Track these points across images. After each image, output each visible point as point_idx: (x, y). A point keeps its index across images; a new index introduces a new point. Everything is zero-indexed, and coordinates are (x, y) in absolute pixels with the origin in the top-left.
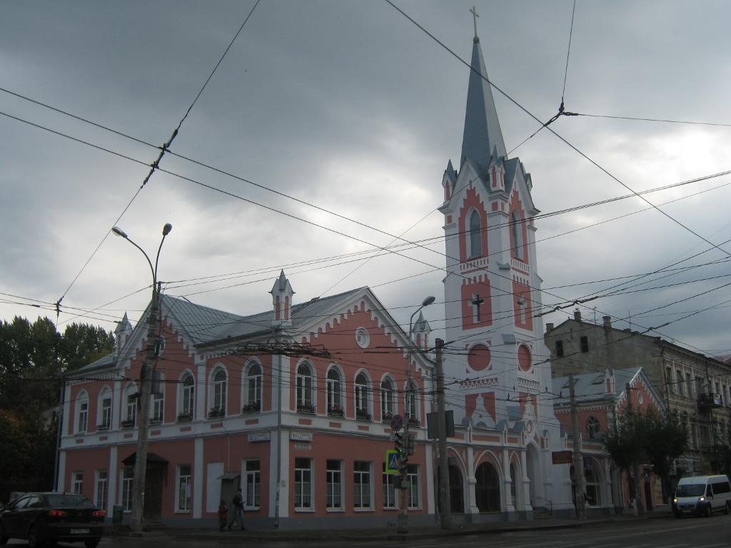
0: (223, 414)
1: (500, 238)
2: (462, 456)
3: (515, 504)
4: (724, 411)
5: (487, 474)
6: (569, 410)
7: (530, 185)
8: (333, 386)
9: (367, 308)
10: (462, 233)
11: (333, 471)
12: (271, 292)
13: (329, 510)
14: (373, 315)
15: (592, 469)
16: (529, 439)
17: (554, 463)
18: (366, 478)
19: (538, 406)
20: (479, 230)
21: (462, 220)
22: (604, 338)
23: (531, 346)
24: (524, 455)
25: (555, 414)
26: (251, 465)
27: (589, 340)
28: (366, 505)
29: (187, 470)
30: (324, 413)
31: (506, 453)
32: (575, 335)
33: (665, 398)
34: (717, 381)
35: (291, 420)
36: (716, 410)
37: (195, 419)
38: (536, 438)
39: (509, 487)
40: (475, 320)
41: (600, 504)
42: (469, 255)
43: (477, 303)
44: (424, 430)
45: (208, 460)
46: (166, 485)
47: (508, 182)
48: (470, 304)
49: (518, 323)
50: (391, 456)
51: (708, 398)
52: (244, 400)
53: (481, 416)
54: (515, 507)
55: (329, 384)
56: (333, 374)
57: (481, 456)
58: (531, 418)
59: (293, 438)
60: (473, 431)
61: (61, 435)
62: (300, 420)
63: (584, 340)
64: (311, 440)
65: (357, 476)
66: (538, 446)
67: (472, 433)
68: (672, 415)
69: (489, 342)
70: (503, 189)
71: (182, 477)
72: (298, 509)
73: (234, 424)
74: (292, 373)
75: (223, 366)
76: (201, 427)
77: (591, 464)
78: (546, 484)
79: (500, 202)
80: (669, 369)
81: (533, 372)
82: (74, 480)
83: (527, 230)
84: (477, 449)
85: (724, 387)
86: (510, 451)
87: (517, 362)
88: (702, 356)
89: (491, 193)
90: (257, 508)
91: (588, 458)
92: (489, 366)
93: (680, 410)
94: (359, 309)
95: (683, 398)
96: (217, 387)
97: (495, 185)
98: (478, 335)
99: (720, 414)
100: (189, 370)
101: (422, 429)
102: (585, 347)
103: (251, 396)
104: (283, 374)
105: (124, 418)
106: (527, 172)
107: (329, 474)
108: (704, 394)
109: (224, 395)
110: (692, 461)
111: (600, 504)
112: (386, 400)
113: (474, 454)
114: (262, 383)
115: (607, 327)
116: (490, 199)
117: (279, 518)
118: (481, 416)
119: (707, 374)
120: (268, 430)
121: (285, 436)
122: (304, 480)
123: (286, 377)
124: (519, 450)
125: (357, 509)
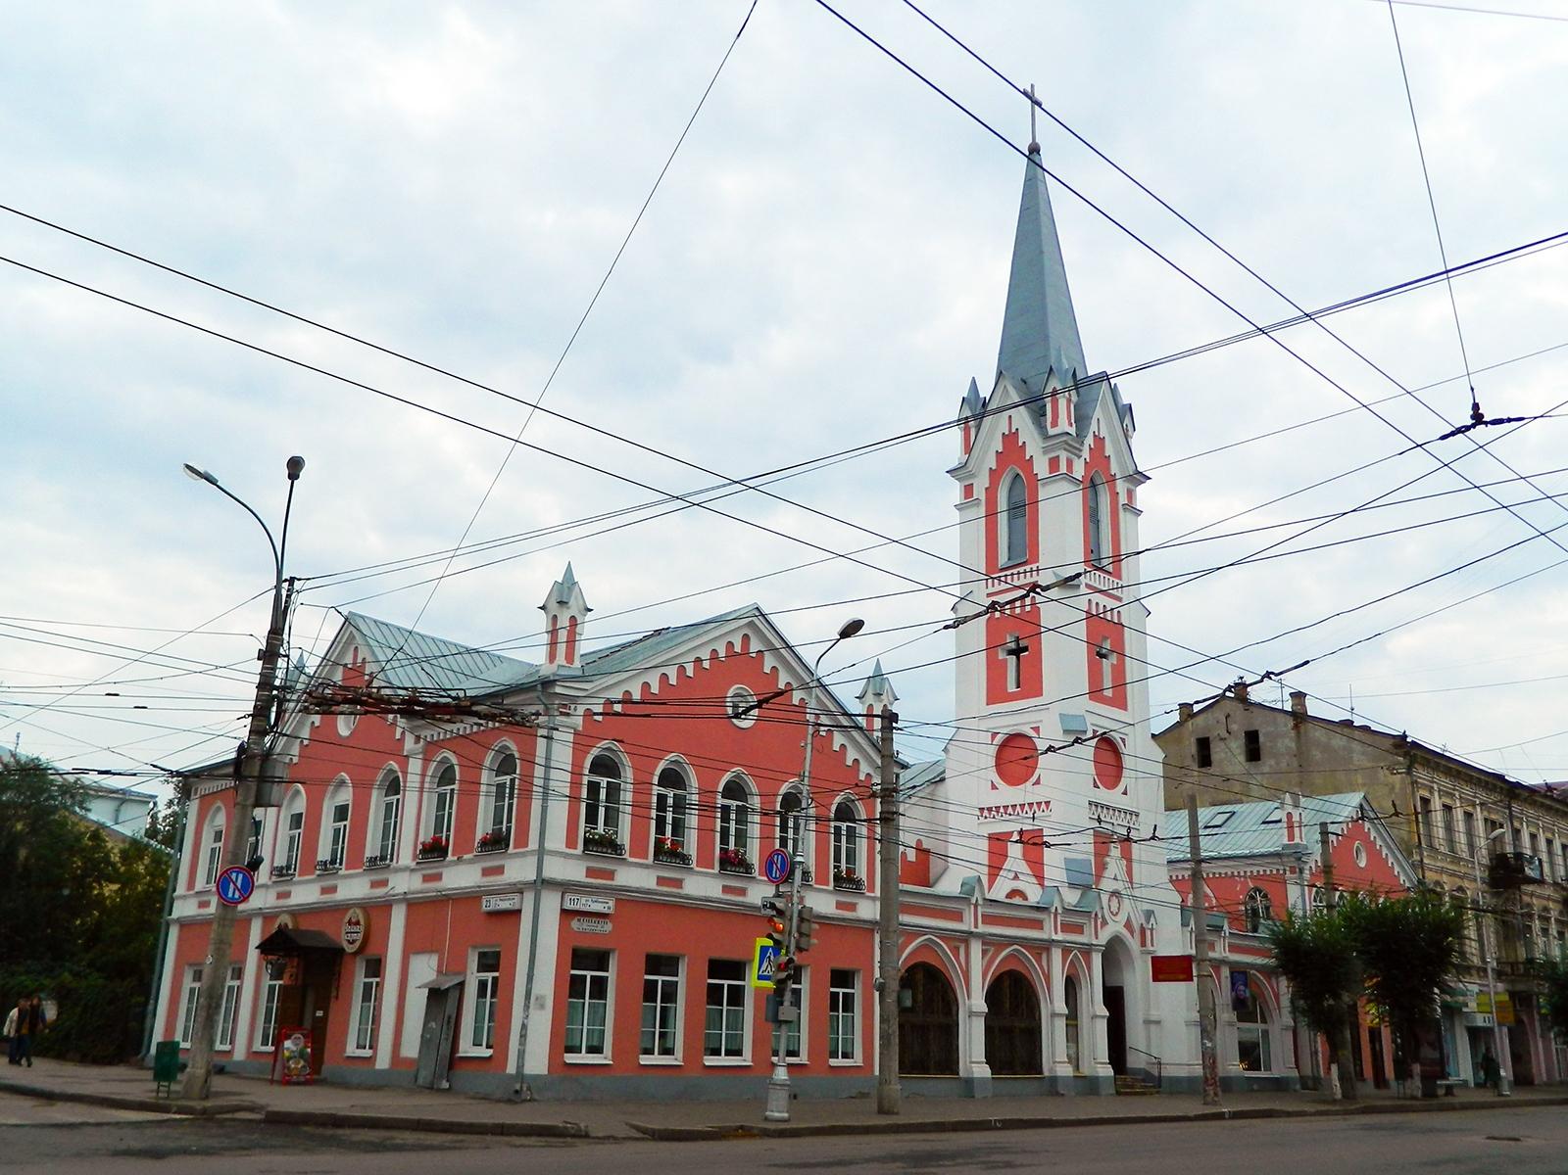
0: (444, 852)
1: (1060, 522)
2: (957, 957)
3: (1075, 1060)
4: (1548, 891)
5: (1013, 998)
6: (1187, 874)
7: (1130, 428)
8: (670, 801)
9: (755, 646)
10: (991, 515)
11: (841, 991)
12: (542, 608)
13: (833, 1062)
14: (769, 662)
15: (1248, 995)
16: (1115, 927)
17: (1155, 979)
18: (670, 994)
19: (1135, 866)
20: (1024, 509)
21: (992, 493)
22: (1293, 733)
23: (1123, 740)
24: (1097, 960)
25: (1171, 881)
26: (489, 962)
27: (1262, 739)
28: (592, 1050)
29: (376, 967)
30: (828, 885)
31: (1057, 955)
32: (1234, 727)
33: (1416, 857)
34: (1533, 830)
35: (574, 870)
36: (1530, 888)
37: (397, 862)
38: (1128, 925)
39: (1061, 1025)
40: (1012, 688)
41: (1268, 1068)
42: (1003, 559)
43: (1016, 652)
44: (874, 899)
45: (410, 950)
46: (337, 998)
47: (1081, 420)
48: (1002, 655)
49: (1096, 693)
50: (764, 949)
51: (1512, 861)
52: (483, 826)
53: (1016, 877)
54: (1077, 1067)
55: (662, 798)
56: (672, 778)
57: (997, 962)
58: (1119, 886)
59: (568, 906)
60: (983, 905)
61: (174, 890)
62: (724, 887)
63: (1252, 738)
64: (611, 911)
65: (650, 987)
66: (1133, 943)
67: (980, 909)
68: (1428, 893)
69: (1036, 729)
70: (1072, 431)
71: (367, 980)
72: (571, 1058)
73: (461, 876)
74: (576, 774)
75: (454, 760)
76: (405, 882)
77: (1246, 985)
78: (1148, 1022)
79: (1063, 456)
80: (1426, 801)
81: (1125, 793)
82: (188, 983)
83: (1122, 514)
84: (991, 943)
85: (1549, 842)
86: (1066, 951)
87: (1091, 768)
88: (1501, 778)
89: (1046, 437)
90: (488, 1053)
91: (1239, 974)
92: (1034, 779)
93: (1448, 884)
94: (738, 649)
95: (1457, 860)
96: (442, 798)
97: (1055, 424)
98: (1013, 717)
99: (1539, 897)
100: (395, 766)
101: (869, 898)
102: (1253, 752)
103: (498, 820)
104: (554, 774)
105: (281, 861)
106: (1125, 401)
107: (650, 987)
108: (1505, 855)
109: (450, 814)
110: (1475, 988)
111: (1268, 1068)
112: (733, 826)
113: (984, 952)
114: (516, 791)
115: (1299, 716)
116: (1046, 450)
117: (523, 1075)
118: (1016, 877)
119: (1510, 813)
120: (518, 889)
121: (551, 904)
122: (843, 1011)
123: (561, 781)
124: (1087, 950)
125: (710, 1061)
